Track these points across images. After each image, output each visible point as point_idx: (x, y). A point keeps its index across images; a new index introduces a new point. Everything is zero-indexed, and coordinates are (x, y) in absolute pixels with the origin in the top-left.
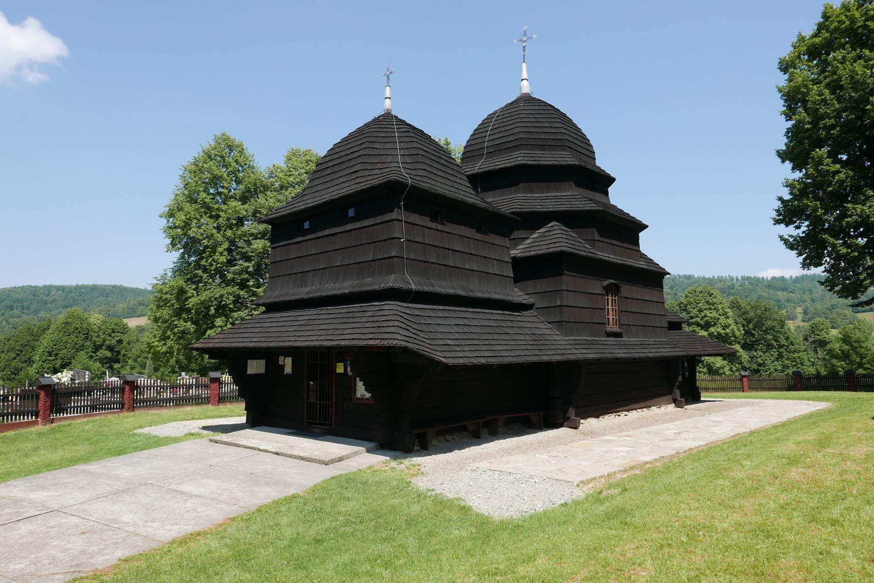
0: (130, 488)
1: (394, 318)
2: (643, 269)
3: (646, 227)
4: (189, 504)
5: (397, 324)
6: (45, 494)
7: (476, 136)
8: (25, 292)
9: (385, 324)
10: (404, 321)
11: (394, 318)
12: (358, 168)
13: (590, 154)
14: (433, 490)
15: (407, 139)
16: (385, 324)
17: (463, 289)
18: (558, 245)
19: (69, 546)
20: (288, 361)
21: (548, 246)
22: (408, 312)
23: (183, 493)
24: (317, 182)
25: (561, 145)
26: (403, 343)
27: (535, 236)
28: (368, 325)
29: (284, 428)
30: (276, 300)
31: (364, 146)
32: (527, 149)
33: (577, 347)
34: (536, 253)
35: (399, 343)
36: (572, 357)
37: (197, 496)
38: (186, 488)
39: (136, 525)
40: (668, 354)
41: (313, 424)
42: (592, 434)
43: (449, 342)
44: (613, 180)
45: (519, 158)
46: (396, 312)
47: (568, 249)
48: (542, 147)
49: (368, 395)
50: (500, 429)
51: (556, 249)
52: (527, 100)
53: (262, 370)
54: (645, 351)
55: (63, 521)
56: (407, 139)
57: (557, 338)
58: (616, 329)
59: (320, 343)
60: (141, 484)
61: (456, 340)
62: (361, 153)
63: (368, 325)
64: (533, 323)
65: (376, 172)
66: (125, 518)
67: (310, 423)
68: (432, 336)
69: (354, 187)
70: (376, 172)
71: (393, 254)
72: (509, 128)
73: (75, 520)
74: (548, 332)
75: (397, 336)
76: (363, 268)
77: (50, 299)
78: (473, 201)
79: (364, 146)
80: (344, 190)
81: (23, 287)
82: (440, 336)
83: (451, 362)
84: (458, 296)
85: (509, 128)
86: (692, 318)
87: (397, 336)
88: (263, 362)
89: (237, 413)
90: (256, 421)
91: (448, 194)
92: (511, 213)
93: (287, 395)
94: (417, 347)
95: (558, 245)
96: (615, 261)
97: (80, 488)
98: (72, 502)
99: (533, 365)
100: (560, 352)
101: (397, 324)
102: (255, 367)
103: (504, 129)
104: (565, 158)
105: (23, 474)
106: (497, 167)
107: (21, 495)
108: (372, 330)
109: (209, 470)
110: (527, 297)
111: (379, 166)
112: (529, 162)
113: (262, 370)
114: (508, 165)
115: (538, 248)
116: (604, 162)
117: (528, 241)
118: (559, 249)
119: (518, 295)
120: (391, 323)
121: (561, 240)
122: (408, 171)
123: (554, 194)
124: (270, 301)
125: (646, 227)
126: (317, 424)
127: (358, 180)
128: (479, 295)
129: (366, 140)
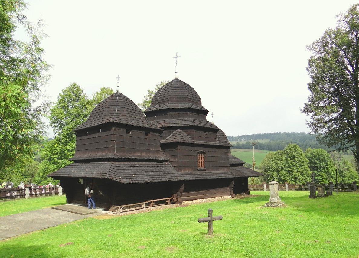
11: (108, 168)
12: (103, 115)
14: (40, 216)
27: (171, 135)
29: (79, 204)
30: (77, 159)
32: (172, 102)
33: (181, 176)
42: (184, 206)
43: (127, 176)
45: (168, 106)
52: (177, 82)
57: (174, 172)
61: (128, 175)
62: (105, 109)
64: (167, 166)
65: (108, 117)
70: (108, 117)
71: (111, 146)
74: (173, 170)
76: (103, 149)
83: (125, 182)
84: (136, 159)
89: (62, 198)
90: (69, 201)
92: (161, 128)
104: (188, 105)
105: (70, 245)
110: (167, 157)
111: (110, 114)
116: (205, 104)
117: (169, 137)
119: (161, 156)
123: (181, 119)
124: (75, 159)
127: (103, 119)
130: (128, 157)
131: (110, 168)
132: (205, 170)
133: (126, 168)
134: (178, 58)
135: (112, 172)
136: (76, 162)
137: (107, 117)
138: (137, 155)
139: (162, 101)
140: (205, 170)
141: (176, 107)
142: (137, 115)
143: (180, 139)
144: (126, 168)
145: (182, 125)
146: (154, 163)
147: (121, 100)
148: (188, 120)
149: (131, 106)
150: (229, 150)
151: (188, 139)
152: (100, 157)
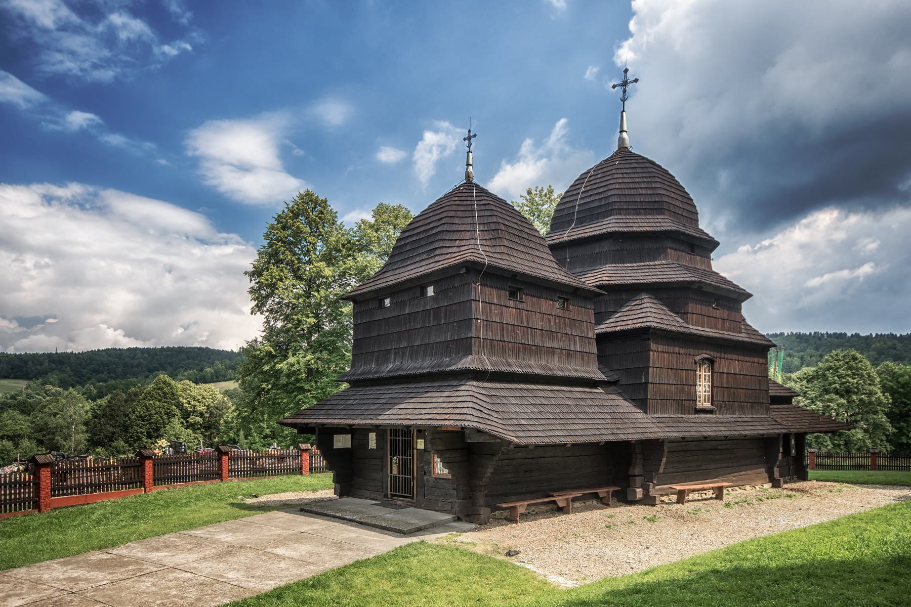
0: (230, 551)
1: (469, 399)
2: (743, 342)
3: (749, 296)
4: (283, 565)
5: (470, 405)
6: (160, 554)
7: (567, 200)
8: (110, 355)
9: (459, 405)
10: (479, 401)
11: (469, 399)
13: (692, 216)
15: (487, 213)
16: (459, 405)
17: (543, 368)
18: (645, 320)
19: (186, 595)
20: (372, 436)
21: (635, 321)
22: (484, 392)
23: (278, 555)
24: (406, 234)
25: (657, 208)
26: (475, 424)
28: (444, 405)
31: (443, 221)
32: (620, 214)
34: (622, 328)
35: (471, 424)
36: (652, 436)
37: (289, 558)
38: (280, 551)
39: (239, 580)
40: (765, 432)
41: (396, 496)
43: (523, 422)
44: (717, 244)
46: (471, 393)
47: (656, 325)
48: (637, 212)
49: (446, 471)
50: (484, 512)
51: (642, 325)
53: (348, 445)
54: (738, 428)
55: (180, 576)
56: (487, 213)
58: (707, 405)
59: (400, 422)
60: (241, 547)
63: (444, 405)
65: (454, 249)
66: (231, 575)
67: (393, 495)
68: (506, 416)
69: (432, 265)
72: (601, 190)
73: (189, 575)
75: (469, 417)
77: (136, 362)
78: (556, 276)
79: (443, 221)
80: (422, 269)
81: (108, 349)
82: (513, 416)
83: (523, 442)
84: (537, 375)
85: (601, 190)
86: (830, 384)
87: (469, 417)
88: (349, 436)
89: (321, 486)
91: (528, 271)
92: (597, 287)
93: (365, 470)
94: (488, 427)
95: (645, 320)
96: (711, 334)
97: (189, 550)
98: (183, 561)
99: (609, 444)
100: (640, 431)
101: (470, 405)
102: (342, 442)
103: (596, 191)
106: (587, 235)
107: (140, 555)
108: (446, 411)
109: (286, 531)
112: (621, 229)
113: (348, 445)
114: (598, 232)
115: (624, 323)
118: (645, 324)
120: (465, 405)
121: (649, 314)
122: (487, 249)
125: (749, 296)
126: (400, 496)
128: (559, 373)
129: (445, 214)
130: (516, 369)
131: (475, 400)
132: (710, 412)
133: (513, 401)
134: (629, 87)
135: (482, 409)
136: (357, 383)
137: (450, 250)
138: (534, 366)
139: (590, 215)
140: (710, 412)
141: (635, 229)
142: (532, 246)
143: (655, 320)
144: (513, 401)
145: (654, 279)
146: (581, 389)
147: (484, 202)
148: (666, 269)
149: (514, 221)
150: (467, 432)
151: (672, 322)
152: (433, 367)
